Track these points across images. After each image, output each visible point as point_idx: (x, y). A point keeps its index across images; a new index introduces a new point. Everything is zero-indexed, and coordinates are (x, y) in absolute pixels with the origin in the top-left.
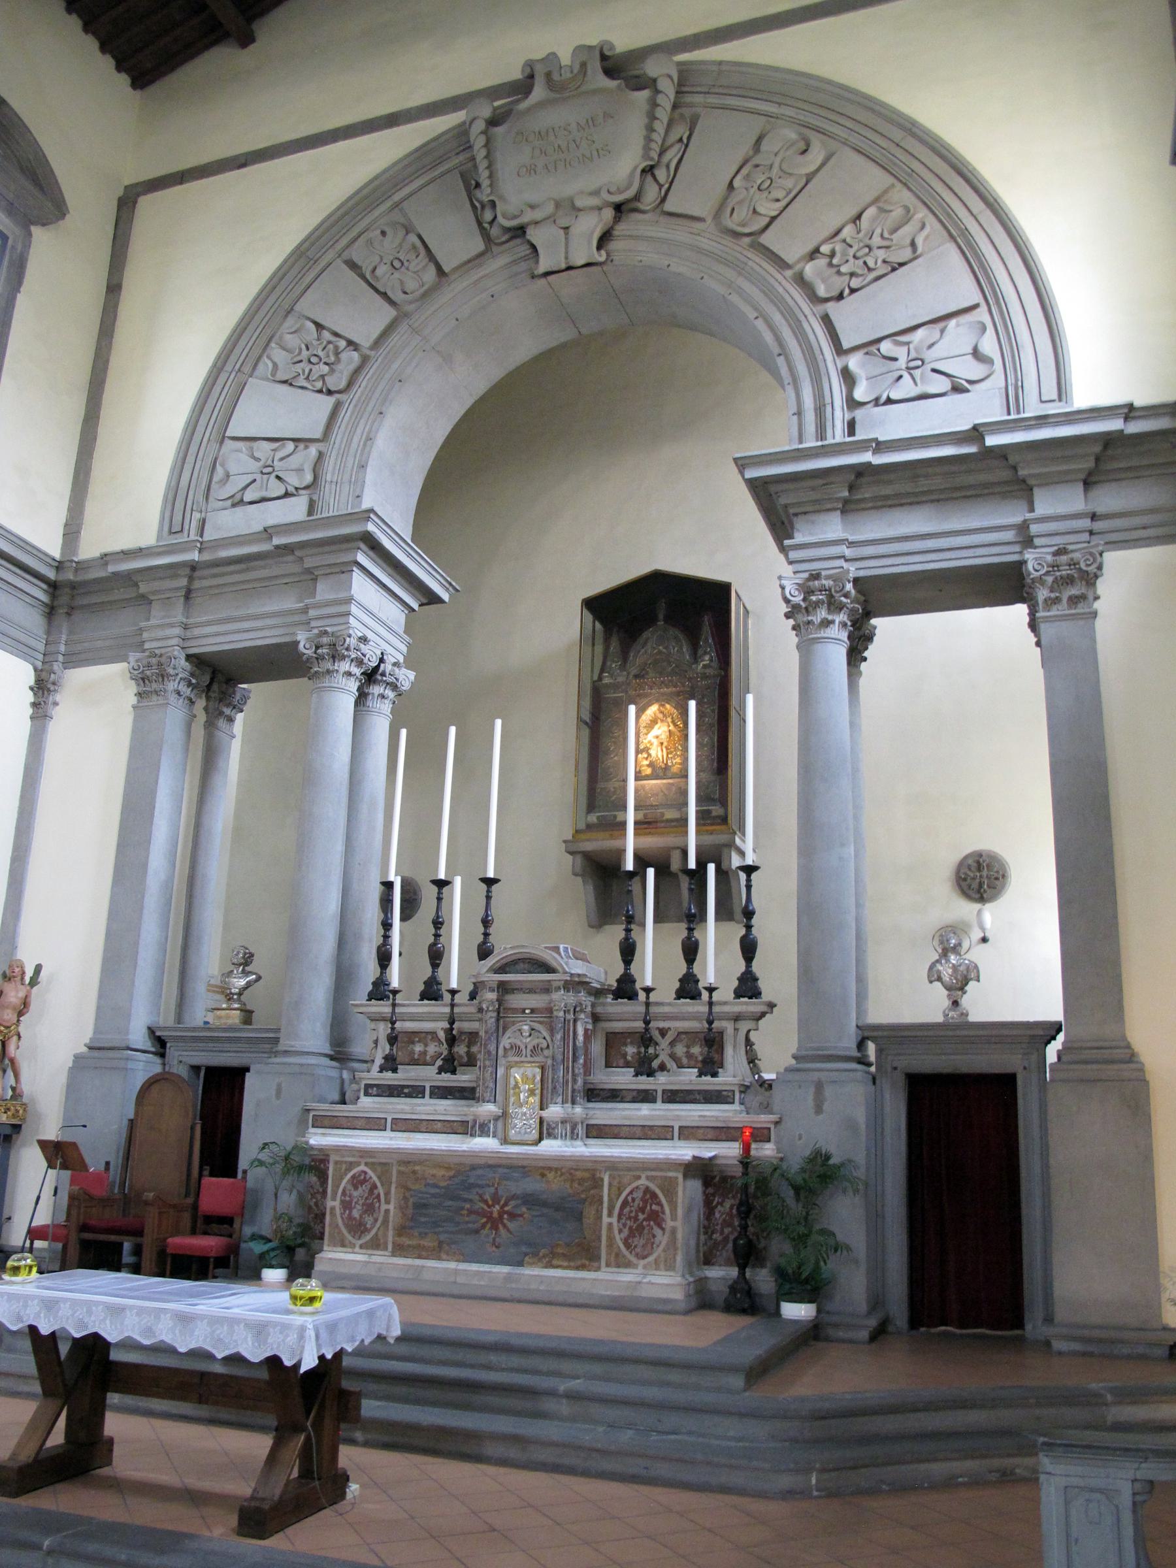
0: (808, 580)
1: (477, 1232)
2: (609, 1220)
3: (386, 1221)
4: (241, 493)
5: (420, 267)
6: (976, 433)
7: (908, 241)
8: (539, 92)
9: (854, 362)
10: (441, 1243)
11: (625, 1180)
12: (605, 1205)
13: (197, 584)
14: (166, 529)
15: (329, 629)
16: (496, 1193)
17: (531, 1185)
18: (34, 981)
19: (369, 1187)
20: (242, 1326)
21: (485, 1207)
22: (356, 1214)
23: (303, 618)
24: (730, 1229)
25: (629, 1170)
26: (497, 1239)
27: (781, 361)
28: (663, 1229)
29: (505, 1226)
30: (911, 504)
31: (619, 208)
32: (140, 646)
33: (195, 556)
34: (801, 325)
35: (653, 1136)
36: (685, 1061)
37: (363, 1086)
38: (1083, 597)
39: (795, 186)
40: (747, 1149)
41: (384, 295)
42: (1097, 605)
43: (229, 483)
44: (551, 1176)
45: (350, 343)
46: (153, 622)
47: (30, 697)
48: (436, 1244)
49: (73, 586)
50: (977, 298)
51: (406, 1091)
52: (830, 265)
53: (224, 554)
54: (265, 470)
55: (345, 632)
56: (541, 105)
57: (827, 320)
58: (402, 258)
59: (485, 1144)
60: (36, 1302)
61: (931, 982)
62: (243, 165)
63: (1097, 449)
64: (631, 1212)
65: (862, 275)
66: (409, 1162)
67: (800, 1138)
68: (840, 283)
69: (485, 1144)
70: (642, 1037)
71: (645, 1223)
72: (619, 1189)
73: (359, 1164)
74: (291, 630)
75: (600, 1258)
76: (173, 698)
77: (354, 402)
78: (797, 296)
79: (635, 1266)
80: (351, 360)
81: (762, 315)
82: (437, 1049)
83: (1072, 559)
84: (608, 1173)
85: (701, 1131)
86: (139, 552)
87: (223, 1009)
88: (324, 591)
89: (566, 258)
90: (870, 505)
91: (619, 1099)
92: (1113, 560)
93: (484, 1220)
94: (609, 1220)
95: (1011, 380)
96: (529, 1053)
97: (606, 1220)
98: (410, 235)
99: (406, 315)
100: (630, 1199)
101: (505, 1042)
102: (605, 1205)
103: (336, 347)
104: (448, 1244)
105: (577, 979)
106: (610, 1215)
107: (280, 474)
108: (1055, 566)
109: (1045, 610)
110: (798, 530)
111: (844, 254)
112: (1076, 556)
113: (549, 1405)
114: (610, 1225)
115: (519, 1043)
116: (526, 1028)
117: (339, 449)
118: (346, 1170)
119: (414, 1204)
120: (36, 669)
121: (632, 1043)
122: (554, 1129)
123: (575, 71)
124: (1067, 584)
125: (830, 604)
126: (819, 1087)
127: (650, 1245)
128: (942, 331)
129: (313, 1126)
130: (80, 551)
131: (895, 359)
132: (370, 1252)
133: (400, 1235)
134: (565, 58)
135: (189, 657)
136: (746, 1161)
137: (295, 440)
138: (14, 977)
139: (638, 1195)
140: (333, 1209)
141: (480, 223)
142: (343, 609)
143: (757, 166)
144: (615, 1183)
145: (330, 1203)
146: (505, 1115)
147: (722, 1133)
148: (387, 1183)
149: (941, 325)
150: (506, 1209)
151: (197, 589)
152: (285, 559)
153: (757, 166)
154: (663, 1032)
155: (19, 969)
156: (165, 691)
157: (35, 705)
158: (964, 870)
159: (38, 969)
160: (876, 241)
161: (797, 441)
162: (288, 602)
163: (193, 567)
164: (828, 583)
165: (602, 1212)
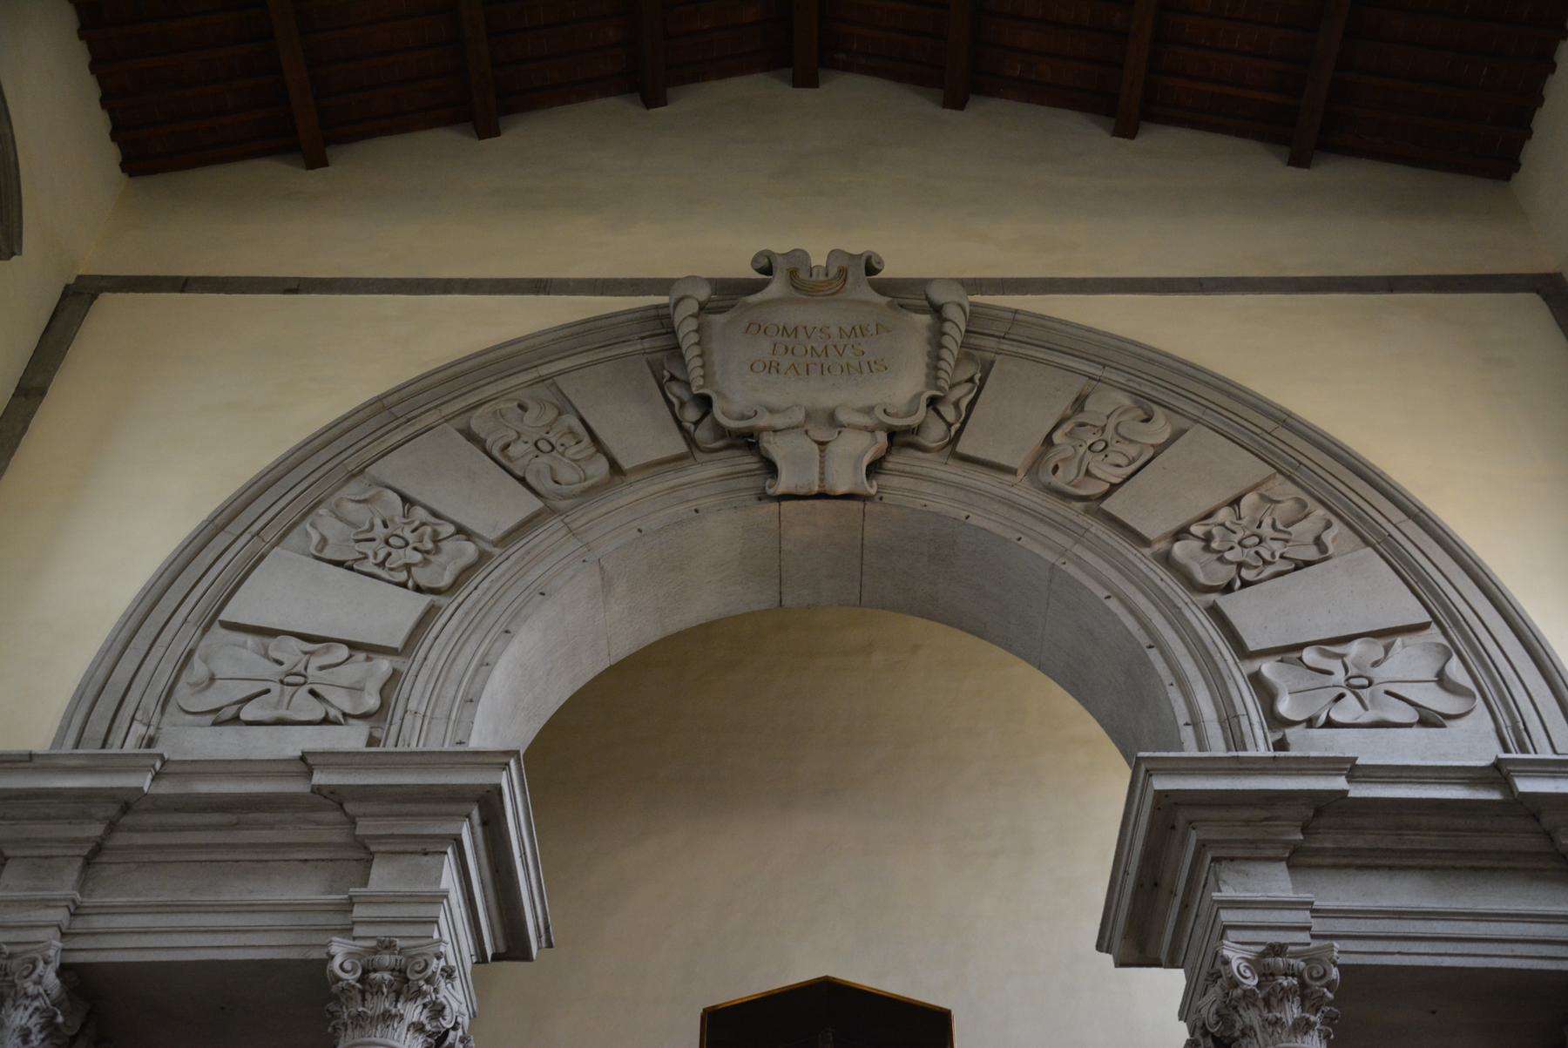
0: (1263, 955)
4: (236, 707)
5: (584, 454)
6: (1498, 774)
7: (1310, 539)
8: (777, 288)
9: (1268, 668)
13: (120, 839)
14: (28, 765)
15: (399, 943)
23: (338, 920)
27: (1154, 655)
30: (1391, 868)
31: (892, 434)
33: (145, 782)
34: (1181, 613)
39: (1140, 455)
41: (522, 480)
43: (211, 690)
45: (461, 530)
55: (432, 950)
57: (1215, 613)
58: (553, 441)
62: (296, 291)
65: (1256, 567)
77: (464, 607)
88: (383, 877)
89: (822, 480)
90: (1329, 861)
95: (1504, 720)
98: (698, 359)
99: (554, 512)
103: (435, 533)
107: (318, 688)
117: (434, 669)
123: (831, 275)
125: (1303, 998)
128: (1387, 649)
134: (818, 259)
135: (64, 970)
137: (353, 646)
141: (679, 423)
143: (1082, 425)
149: (1388, 640)
152: (318, 816)
153: (1082, 425)
162: (309, 890)
163: (127, 803)
164: (1300, 964)
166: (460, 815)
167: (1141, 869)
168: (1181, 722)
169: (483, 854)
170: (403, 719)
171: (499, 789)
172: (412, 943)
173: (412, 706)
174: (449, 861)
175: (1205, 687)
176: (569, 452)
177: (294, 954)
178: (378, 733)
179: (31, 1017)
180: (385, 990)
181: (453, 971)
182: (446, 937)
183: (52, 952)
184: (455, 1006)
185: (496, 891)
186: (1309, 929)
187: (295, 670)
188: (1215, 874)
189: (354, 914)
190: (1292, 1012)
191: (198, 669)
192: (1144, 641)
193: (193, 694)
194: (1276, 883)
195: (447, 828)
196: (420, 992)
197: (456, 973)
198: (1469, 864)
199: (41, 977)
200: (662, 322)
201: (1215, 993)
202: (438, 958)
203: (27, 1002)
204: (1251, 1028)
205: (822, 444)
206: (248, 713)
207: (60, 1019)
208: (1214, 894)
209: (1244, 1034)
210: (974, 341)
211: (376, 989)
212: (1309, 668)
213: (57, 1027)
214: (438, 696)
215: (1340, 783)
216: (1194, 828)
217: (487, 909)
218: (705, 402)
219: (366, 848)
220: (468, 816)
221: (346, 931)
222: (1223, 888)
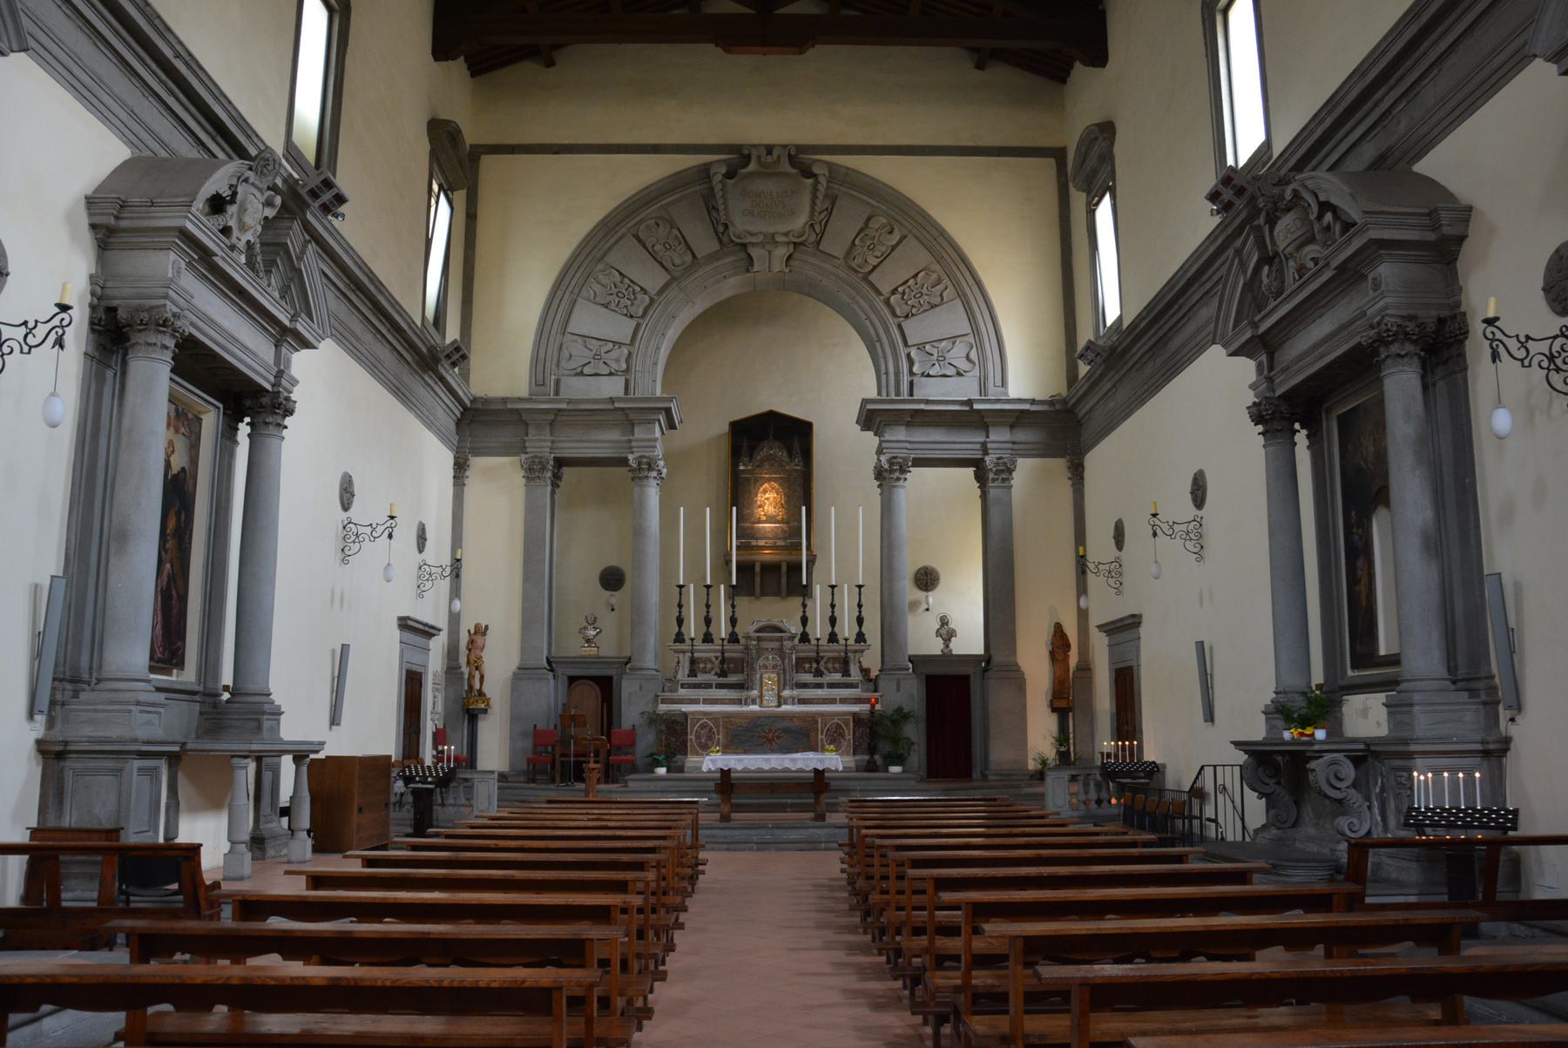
6: (970, 402)
13: (558, 418)
17: (787, 724)
23: (628, 445)
27: (878, 345)
33: (564, 406)
38: (1008, 479)
41: (661, 264)
42: (1012, 482)
45: (642, 289)
47: (451, 473)
50: (970, 331)
52: (903, 298)
53: (582, 407)
56: (751, 174)
57: (900, 327)
59: (755, 708)
68: (906, 309)
69: (755, 708)
78: (886, 311)
80: (643, 301)
81: (868, 318)
86: (521, 400)
88: (639, 433)
92: (1020, 461)
101: (761, 662)
103: (634, 290)
111: (910, 294)
128: (954, 343)
136: (872, 712)
141: (716, 232)
145: (689, 737)
146: (761, 696)
147: (858, 701)
148: (718, 727)
154: (822, 658)
157: (454, 477)
158: (931, 574)
159: (487, 627)
160: (924, 291)
162: (615, 435)
164: (901, 460)
174: (657, 425)
176: (678, 249)
177: (617, 455)
191: (565, 353)
192: (875, 338)
200: (705, 172)
205: (770, 252)
206: (587, 370)
210: (831, 185)
211: (643, 469)
218: (726, 226)
221: (632, 453)
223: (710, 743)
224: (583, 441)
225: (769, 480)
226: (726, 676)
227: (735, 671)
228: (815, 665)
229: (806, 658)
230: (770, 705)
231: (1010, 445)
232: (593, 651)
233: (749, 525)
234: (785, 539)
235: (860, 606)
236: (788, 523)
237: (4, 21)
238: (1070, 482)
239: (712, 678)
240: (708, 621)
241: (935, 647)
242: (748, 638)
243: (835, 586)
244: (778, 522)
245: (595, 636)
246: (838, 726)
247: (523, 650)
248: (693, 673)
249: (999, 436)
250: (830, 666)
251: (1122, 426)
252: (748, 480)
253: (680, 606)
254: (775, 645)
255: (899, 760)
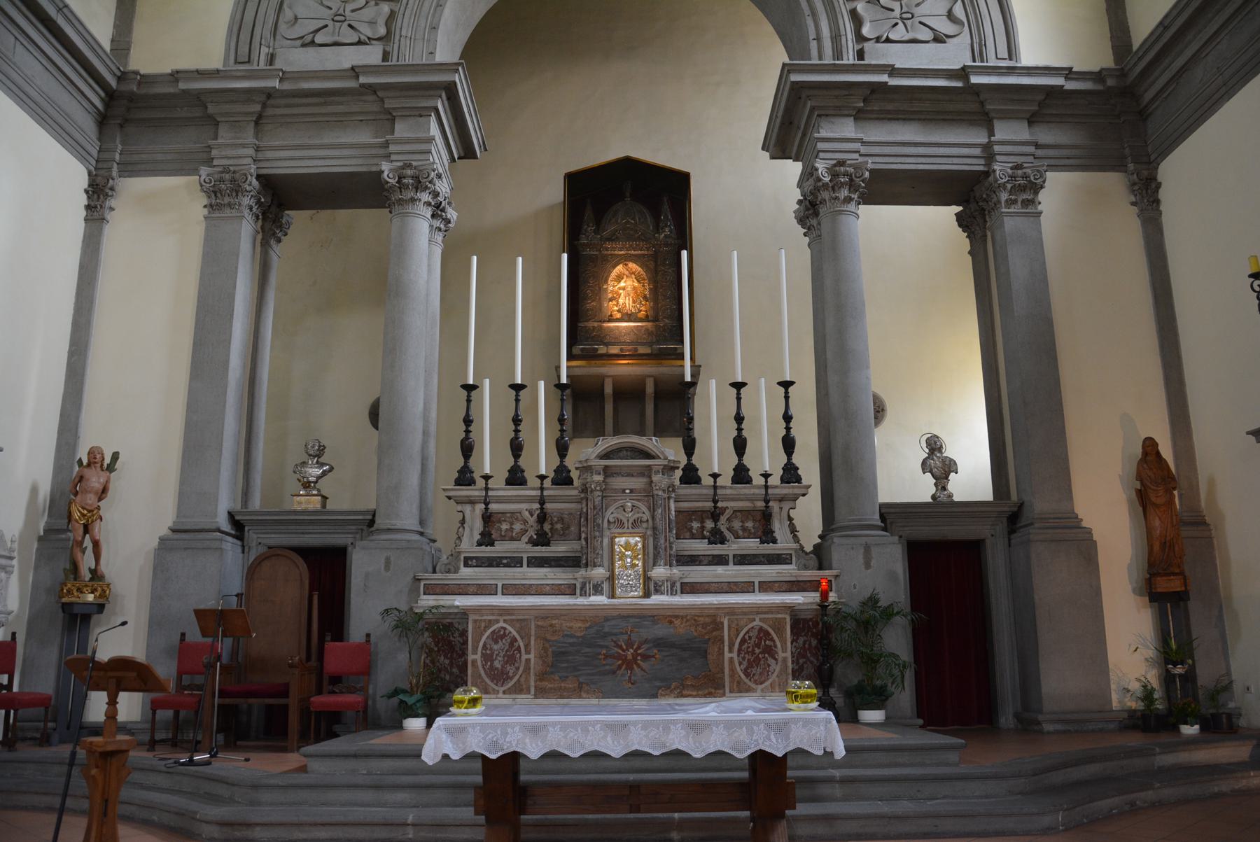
0: (835, 165)
1: (614, 672)
2: (731, 655)
3: (527, 668)
4: (312, 35)
6: (963, 73)
10: (581, 684)
11: (742, 623)
12: (726, 643)
13: (269, 112)
16: (629, 639)
17: (661, 631)
18: (111, 468)
19: (509, 641)
20: (762, 726)
21: (621, 652)
22: (497, 664)
23: (382, 152)
24: (804, 660)
25: (745, 614)
26: (633, 678)
28: (776, 659)
29: (639, 666)
30: (904, 119)
32: (209, 162)
33: (276, 84)
35: (738, 590)
36: (740, 533)
37: (462, 558)
40: (825, 596)
42: (1040, 208)
43: (297, 25)
44: (677, 622)
46: (220, 141)
47: (83, 200)
48: (576, 685)
49: (132, 98)
51: (505, 561)
53: (306, 85)
54: (337, 18)
60: (517, 729)
61: (924, 473)
63: (1041, 97)
64: (749, 647)
66: (547, 618)
67: (855, 588)
70: (764, 513)
71: (760, 656)
72: (737, 630)
73: (497, 621)
74: (375, 161)
75: (724, 687)
76: (246, 212)
79: (754, 690)
82: (523, 527)
83: (1025, 173)
84: (727, 618)
85: (776, 585)
86: (201, 74)
87: (302, 495)
88: (402, 129)
91: (697, 563)
93: (620, 662)
94: (731, 655)
95: (976, 39)
96: (630, 525)
97: (727, 655)
100: (747, 637)
101: (610, 515)
102: (726, 643)
104: (587, 684)
105: (672, 465)
106: (731, 651)
107: (353, 23)
108: (1013, 177)
109: (1006, 208)
110: (822, 128)
112: (1029, 171)
113: (824, 790)
114: (731, 660)
115: (621, 517)
116: (629, 504)
118: (485, 627)
119: (553, 652)
120: (90, 174)
121: (695, 520)
122: (660, 586)
124: (1021, 191)
126: (867, 548)
127: (766, 673)
129: (424, 594)
130: (131, 64)
131: (893, 10)
132: (514, 696)
133: (541, 680)
135: (259, 177)
136: (823, 606)
138: (95, 463)
139: (754, 634)
140: (474, 662)
142: (423, 147)
144: (734, 625)
145: (471, 657)
146: (612, 578)
148: (526, 636)
150: (639, 652)
151: (267, 116)
154: (724, 509)
155: (100, 455)
156: (240, 205)
157: (88, 207)
159: (115, 456)
161: (817, 58)
162: (364, 136)
163: (269, 94)
164: (851, 170)
165: (723, 649)
166: (436, 96)
167: (783, 116)
168: (811, 38)
169: (449, 113)
170: (400, 41)
171: (455, 83)
172: (420, 163)
173: (404, 33)
174: (433, 118)
175: (826, 17)
178: (388, 49)
179: (250, 199)
180: (410, 187)
181: (441, 175)
182: (437, 161)
183: (252, 171)
184: (444, 190)
185: (457, 129)
186: (859, 152)
187: (339, 13)
188: (818, 123)
189: (390, 149)
190: (844, 193)
191: (288, 14)
193: (288, 28)
194: (847, 128)
195: (430, 103)
196: (426, 188)
197: (443, 175)
198: (942, 117)
199: (251, 182)
201: (811, 181)
202: (434, 171)
203: (248, 194)
204: (825, 200)
206: (319, 39)
207: (263, 200)
208: (816, 135)
209: (821, 203)
212: (882, 7)
213: (262, 203)
214: (417, 26)
215: (884, 78)
216: (810, 99)
217: (453, 137)
219: (390, 114)
220: (440, 96)
221: (387, 157)
222: (821, 131)
223: (510, 669)
224: (309, 147)
225: (624, 259)
226: (548, 544)
227: (564, 536)
228: (709, 524)
229: (694, 512)
230: (630, 597)
231: (1031, 149)
232: (314, 503)
233: (596, 324)
234: (650, 344)
235: (787, 418)
236: (655, 320)
237: (2, 58)
238: (1135, 210)
239: (522, 547)
240: (516, 448)
241: (921, 489)
242: (586, 469)
243: (743, 384)
244: (640, 320)
245: (319, 478)
246: (763, 634)
247: (182, 497)
248: (486, 539)
249: (1009, 132)
250: (737, 525)
251: (1222, 110)
252: (593, 259)
253: (468, 421)
254: (638, 483)
255: (878, 698)
